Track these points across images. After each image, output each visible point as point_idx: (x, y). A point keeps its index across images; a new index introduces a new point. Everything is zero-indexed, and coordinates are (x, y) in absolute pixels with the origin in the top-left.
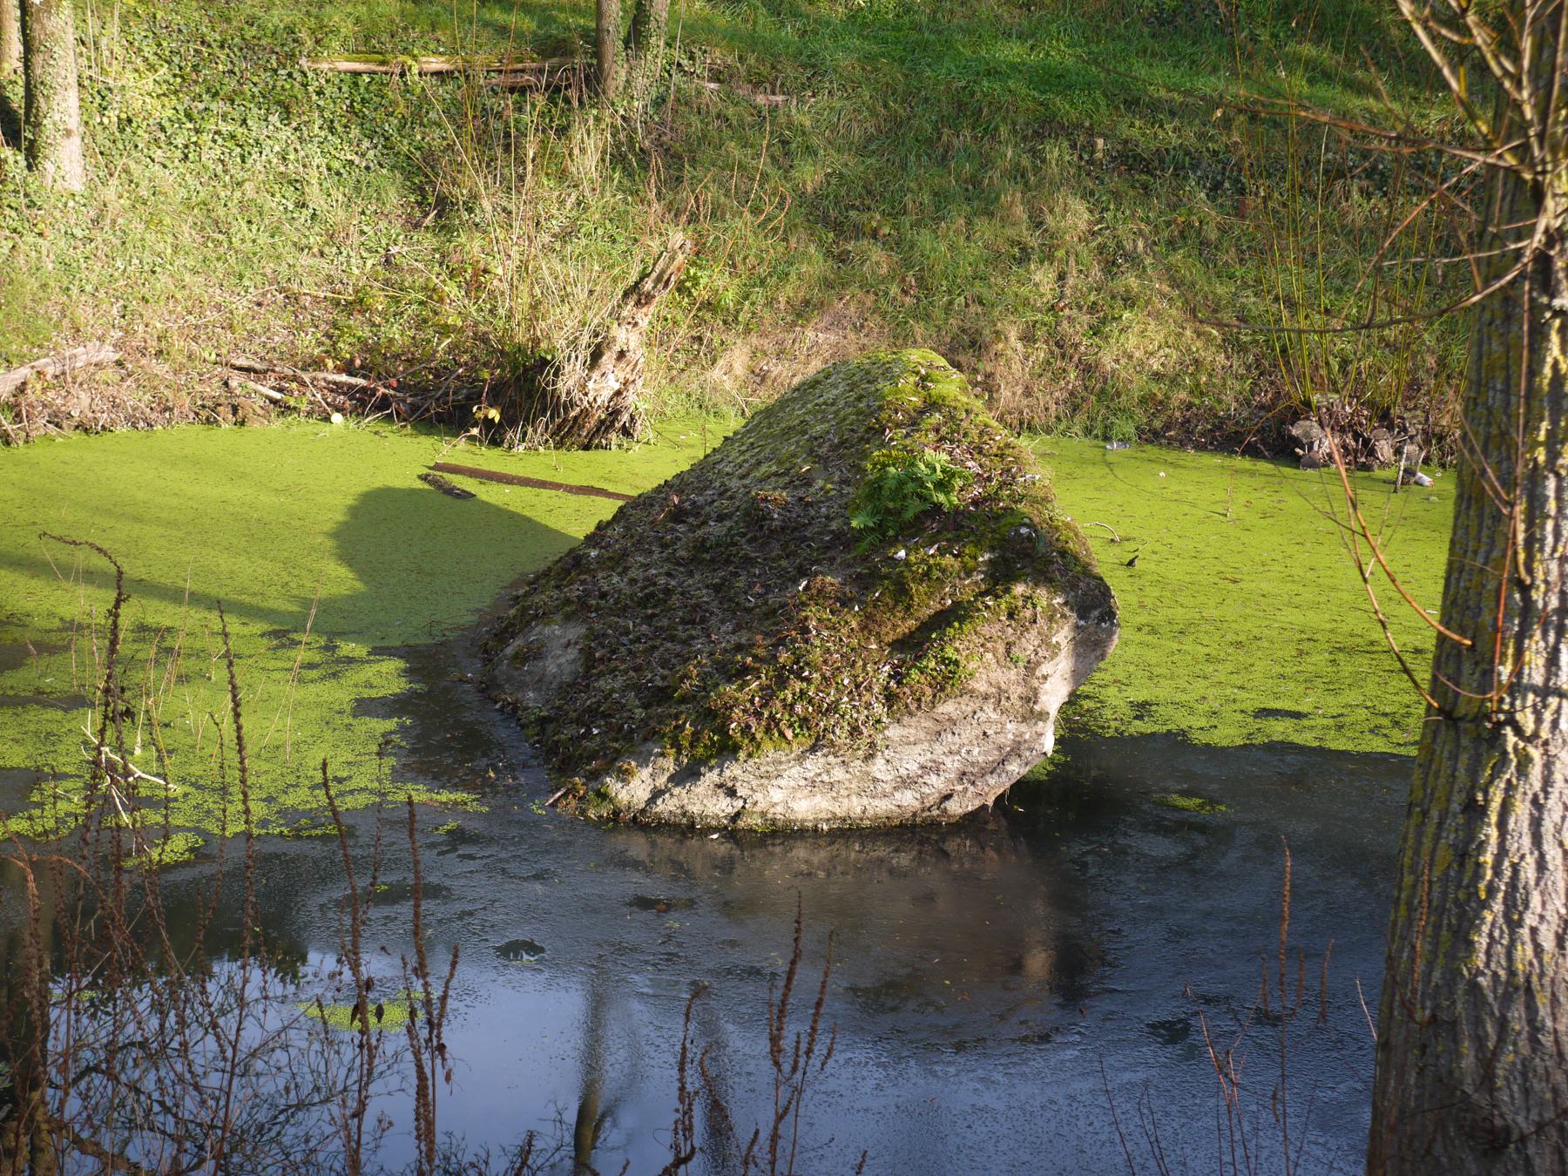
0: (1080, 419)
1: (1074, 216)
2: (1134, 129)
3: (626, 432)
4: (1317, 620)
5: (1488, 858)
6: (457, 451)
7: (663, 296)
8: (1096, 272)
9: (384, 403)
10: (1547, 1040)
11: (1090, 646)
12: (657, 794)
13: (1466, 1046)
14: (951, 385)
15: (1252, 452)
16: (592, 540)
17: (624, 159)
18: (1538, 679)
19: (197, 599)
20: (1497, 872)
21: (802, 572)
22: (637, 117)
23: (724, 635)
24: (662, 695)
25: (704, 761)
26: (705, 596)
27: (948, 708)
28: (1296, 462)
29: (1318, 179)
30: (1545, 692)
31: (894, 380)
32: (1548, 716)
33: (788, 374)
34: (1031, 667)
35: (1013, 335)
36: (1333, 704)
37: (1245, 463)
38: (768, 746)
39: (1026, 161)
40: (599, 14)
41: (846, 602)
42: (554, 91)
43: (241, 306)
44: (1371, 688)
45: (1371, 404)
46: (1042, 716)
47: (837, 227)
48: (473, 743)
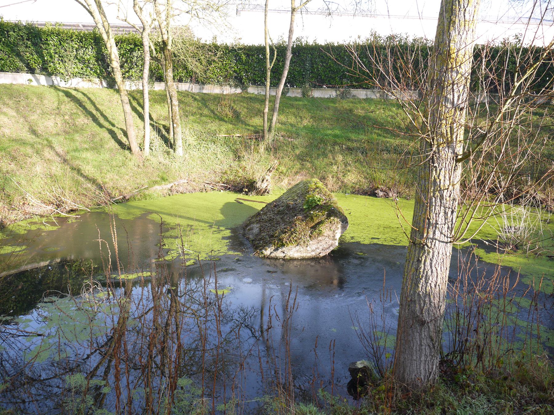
0: (341, 190)
1: (340, 158)
2: (349, 144)
3: (268, 193)
4: (381, 223)
5: (422, 270)
6: (241, 196)
7: (274, 171)
8: (343, 166)
9: (229, 188)
10: (433, 304)
11: (344, 228)
12: (271, 253)
13: (417, 305)
14: (320, 184)
15: (369, 195)
16: (261, 210)
17: (268, 149)
18: (431, 237)
19: (197, 220)
20: (423, 273)
21: (296, 215)
22: (270, 143)
23: (283, 226)
24: (272, 236)
25: (279, 247)
26: (279, 219)
27: (320, 238)
28: (376, 197)
29: (379, 152)
30: (433, 239)
31: (311, 183)
32: (433, 244)
33: (293, 183)
34: (334, 231)
35: (330, 177)
36: (384, 237)
37: (368, 197)
38: (290, 245)
39: (332, 149)
40: (264, 127)
41: (303, 220)
42: (256, 139)
43: (207, 173)
44: (390, 234)
45: (388, 187)
46: (336, 239)
47: (302, 160)
48: (241, 244)
